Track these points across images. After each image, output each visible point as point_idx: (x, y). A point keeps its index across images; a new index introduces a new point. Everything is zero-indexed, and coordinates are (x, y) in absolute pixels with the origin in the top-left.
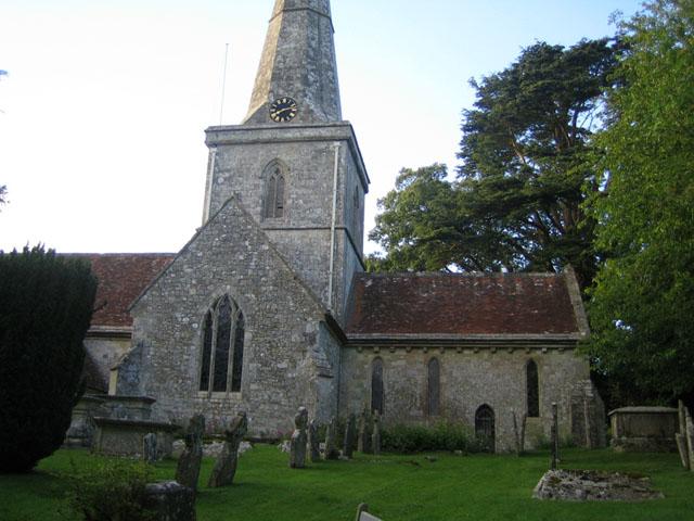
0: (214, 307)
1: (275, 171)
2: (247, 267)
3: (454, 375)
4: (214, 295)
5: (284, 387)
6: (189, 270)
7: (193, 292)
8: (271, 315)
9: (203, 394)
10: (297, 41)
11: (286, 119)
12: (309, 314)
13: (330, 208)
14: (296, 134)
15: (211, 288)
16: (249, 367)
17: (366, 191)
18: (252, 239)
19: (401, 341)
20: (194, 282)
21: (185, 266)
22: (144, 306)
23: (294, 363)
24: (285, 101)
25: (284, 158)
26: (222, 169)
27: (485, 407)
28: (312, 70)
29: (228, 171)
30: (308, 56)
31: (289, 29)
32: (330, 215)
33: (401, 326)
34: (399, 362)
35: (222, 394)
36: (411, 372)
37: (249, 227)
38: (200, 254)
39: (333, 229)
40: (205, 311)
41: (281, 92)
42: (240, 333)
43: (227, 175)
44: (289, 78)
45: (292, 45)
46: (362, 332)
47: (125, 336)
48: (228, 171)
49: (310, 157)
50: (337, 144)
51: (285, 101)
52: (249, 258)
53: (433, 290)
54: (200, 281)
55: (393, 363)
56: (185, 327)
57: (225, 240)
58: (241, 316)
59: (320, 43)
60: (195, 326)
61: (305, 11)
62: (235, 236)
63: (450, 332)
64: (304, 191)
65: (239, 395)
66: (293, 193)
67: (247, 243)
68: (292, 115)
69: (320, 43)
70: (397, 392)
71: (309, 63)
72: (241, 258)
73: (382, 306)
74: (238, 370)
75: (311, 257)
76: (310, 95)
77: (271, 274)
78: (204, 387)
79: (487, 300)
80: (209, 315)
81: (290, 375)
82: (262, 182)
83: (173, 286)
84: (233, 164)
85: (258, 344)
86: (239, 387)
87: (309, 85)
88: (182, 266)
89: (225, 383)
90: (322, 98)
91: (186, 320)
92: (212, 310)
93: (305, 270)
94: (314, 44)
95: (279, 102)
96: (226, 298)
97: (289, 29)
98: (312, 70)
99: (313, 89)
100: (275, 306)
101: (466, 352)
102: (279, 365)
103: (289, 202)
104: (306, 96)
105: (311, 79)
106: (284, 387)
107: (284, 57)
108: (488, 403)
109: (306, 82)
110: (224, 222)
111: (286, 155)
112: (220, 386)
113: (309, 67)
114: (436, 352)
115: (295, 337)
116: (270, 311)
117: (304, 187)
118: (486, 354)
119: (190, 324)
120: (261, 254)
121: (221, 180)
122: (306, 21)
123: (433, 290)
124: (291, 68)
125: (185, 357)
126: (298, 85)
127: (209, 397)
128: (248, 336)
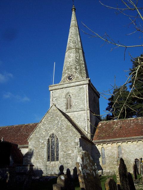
0: (50, 137)
1: (68, 95)
2: (58, 125)
3: (126, 150)
4: (50, 134)
5: (71, 159)
6: (43, 127)
7: (44, 133)
8: (66, 138)
9: (48, 162)
10: (73, 58)
11: (71, 80)
12: (76, 136)
13: (85, 104)
14: (61, 87)
15: (49, 132)
16: (61, 153)
17: (99, 97)
18: (59, 116)
19: (109, 141)
20: (44, 130)
21: (41, 126)
22: (31, 138)
23: (73, 151)
24: (70, 75)
25: (71, 91)
26: (54, 97)
27: (136, 159)
28: (78, 65)
29: (56, 97)
30: (76, 61)
31: (70, 55)
32: (85, 106)
33: (116, 137)
34: (109, 148)
35: (54, 162)
36: (113, 151)
37: (58, 113)
38: (45, 122)
39: (86, 110)
40: (48, 139)
41: (69, 73)
42: (57, 144)
43: (56, 98)
44: (71, 68)
45: (72, 59)
46: (98, 140)
47: (27, 147)
48: (56, 97)
49: (78, 90)
50: (85, 85)
51: (70, 75)
52: (58, 122)
53: (119, 125)
54: (46, 130)
55: (107, 148)
56: (43, 143)
57: (52, 118)
58: (57, 139)
59: (79, 57)
60: (45, 143)
61: (75, 49)
62: (54, 116)
63: (124, 137)
64: (77, 100)
65: (58, 162)
66: (74, 102)
67: (58, 118)
68: (73, 79)
69: (79, 57)
70: (109, 157)
71: (77, 63)
72: (56, 122)
73: (104, 131)
74: (58, 155)
75: (81, 119)
76: (78, 72)
77: (65, 126)
78: (48, 160)
79: (135, 126)
80: (49, 139)
81: (72, 155)
82: (65, 99)
83: (39, 132)
84: (57, 95)
85: (63, 147)
86: (58, 159)
87: (77, 70)
88: (40, 126)
89: (54, 159)
90: (81, 73)
91: (43, 141)
92: (49, 138)
93: (79, 123)
94: (77, 58)
95: (69, 76)
96: (53, 134)
97: (70, 55)
98: (78, 65)
99: (78, 70)
100: (66, 135)
101: (129, 143)
102: (69, 152)
103: (73, 104)
104: (76, 73)
105: (77, 68)
106: (71, 159)
107: (69, 63)
108: (137, 158)
109: (76, 69)
110: (51, 112)
111: (71, 90)
112: (53, 160)
113: (77, 64)
114: (120, 144)
115: (73, 144)
116: (65, 137)
117: (77, 99)
118: (135, 143)
119: (44, 142)
120: (62, 121)
121: (54, 100)
122: (75, 51)
123: (119, 125)
124: (71, 65)
125: (43, 152)
126: (74, 70)
127: (50, 163)
128: (60, 144)
